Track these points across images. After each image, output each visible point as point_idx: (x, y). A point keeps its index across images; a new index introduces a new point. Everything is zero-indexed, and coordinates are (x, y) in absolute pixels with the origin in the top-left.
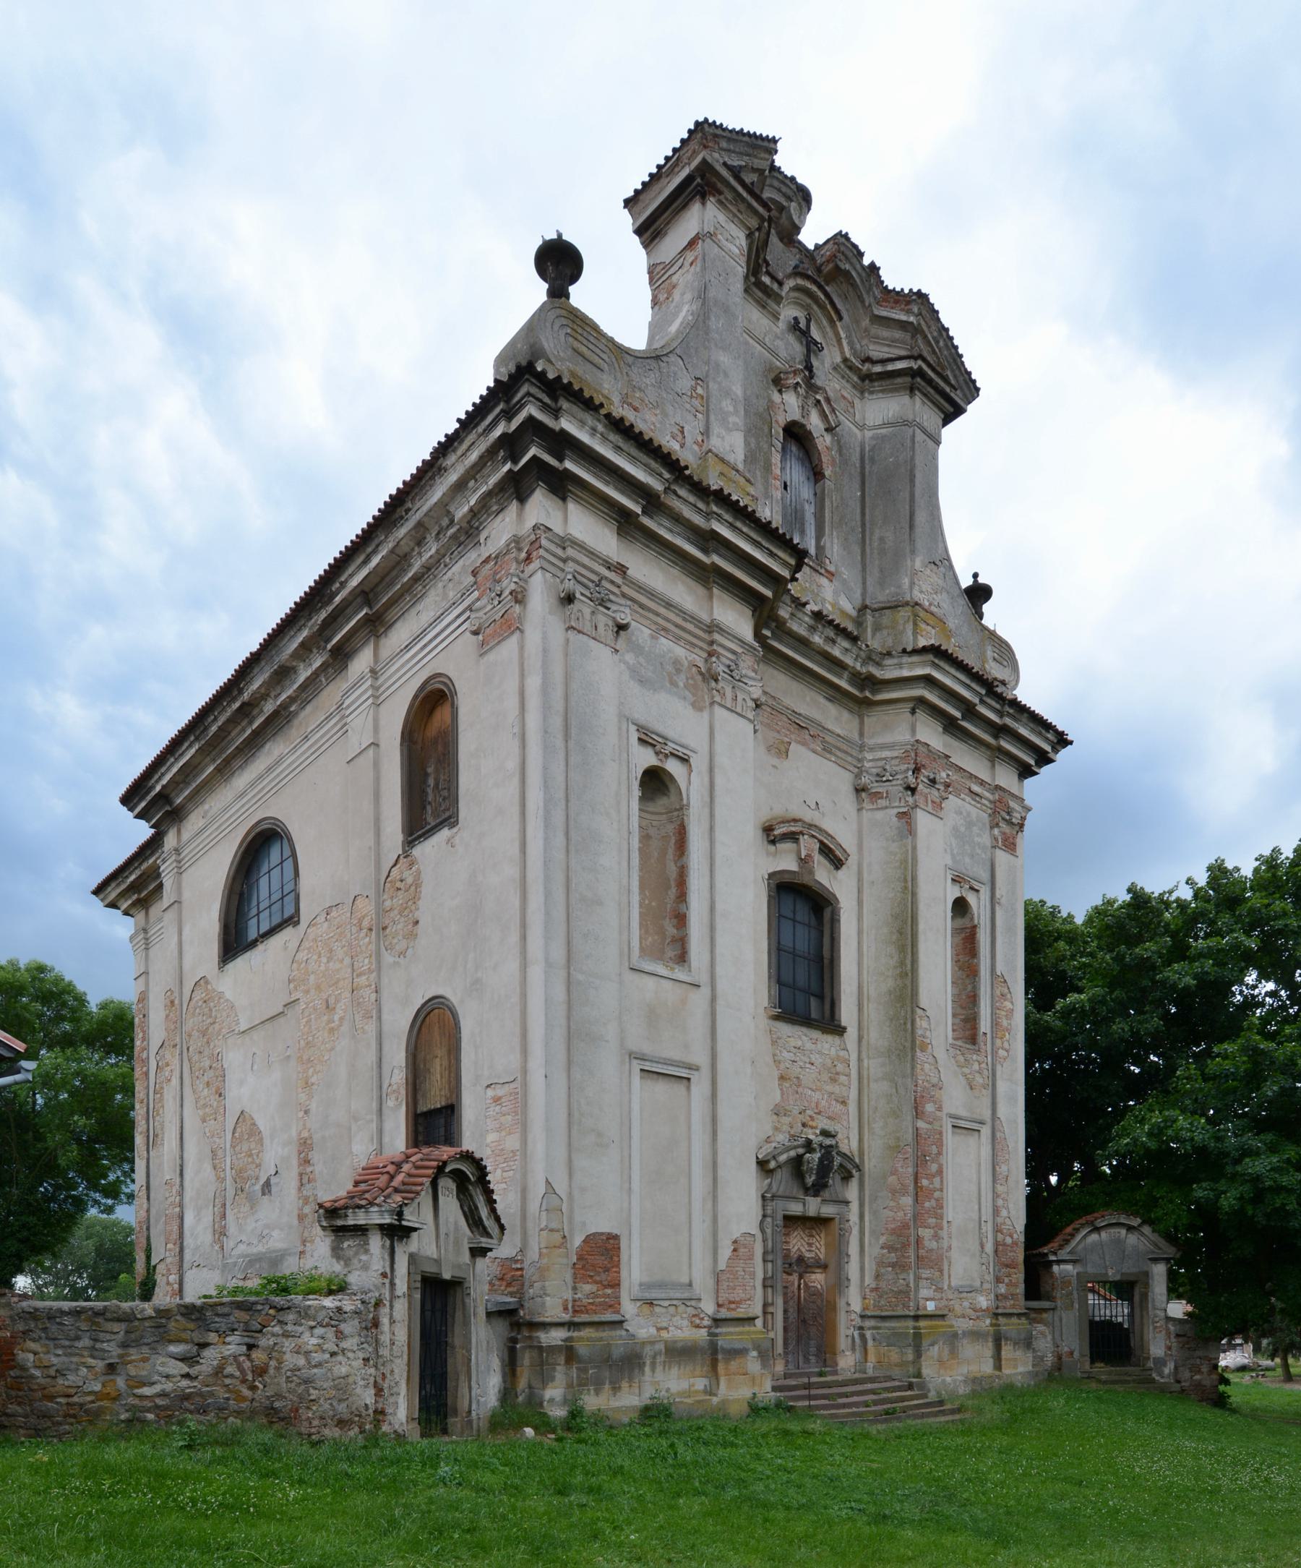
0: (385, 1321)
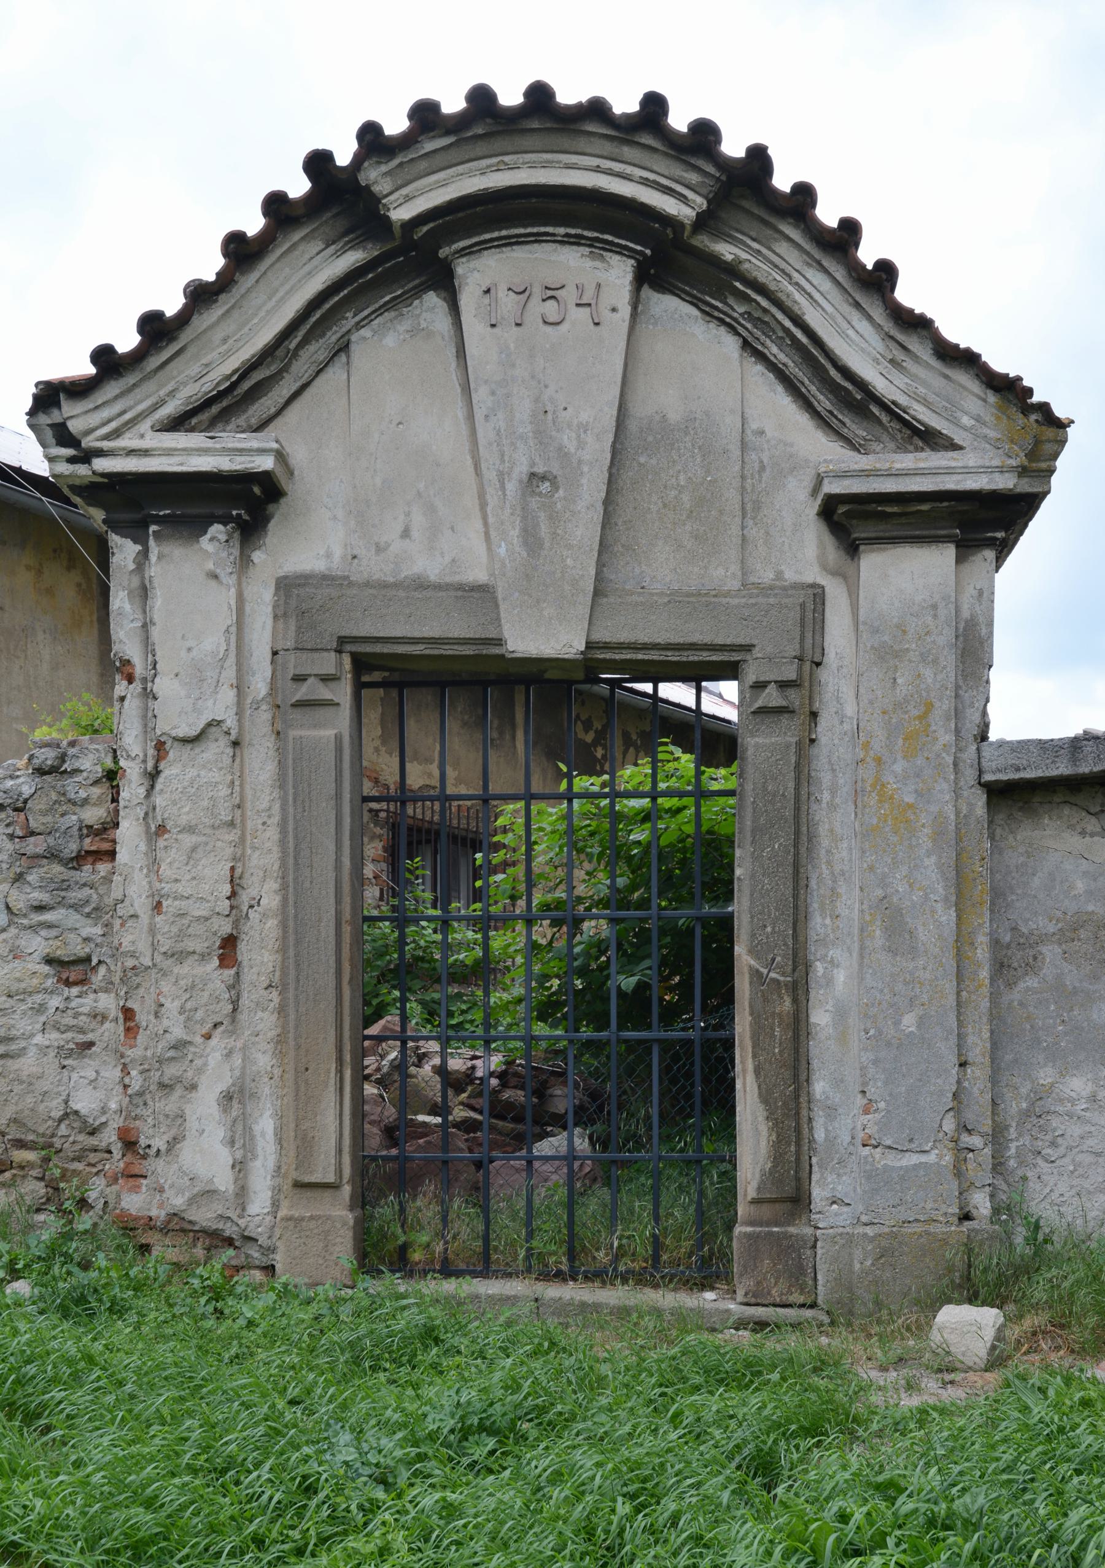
0: (129, 835)
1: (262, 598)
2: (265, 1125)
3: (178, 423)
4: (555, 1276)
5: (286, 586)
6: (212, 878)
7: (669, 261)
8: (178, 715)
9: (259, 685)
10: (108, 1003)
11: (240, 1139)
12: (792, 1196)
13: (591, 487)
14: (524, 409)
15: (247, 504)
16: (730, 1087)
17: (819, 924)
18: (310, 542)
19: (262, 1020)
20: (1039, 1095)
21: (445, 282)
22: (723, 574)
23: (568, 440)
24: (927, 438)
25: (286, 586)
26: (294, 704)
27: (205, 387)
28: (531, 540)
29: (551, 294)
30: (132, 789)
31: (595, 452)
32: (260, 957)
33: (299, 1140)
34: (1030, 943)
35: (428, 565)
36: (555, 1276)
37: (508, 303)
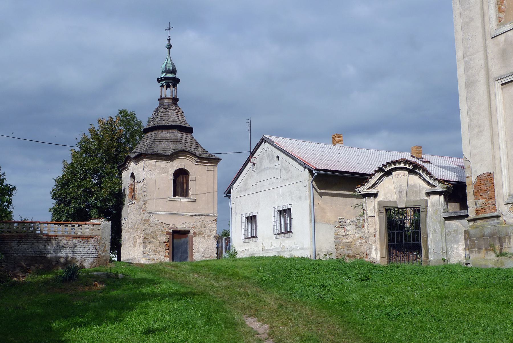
1: (376, 203)
2: (379, 252)
3: (368, 189)
4: (432, 177)
5: (378, 202)
6: (373, 229)
7: (411, 172)
8: (369, 215)
9: (377, 211)
10: (364, 241)
11: (376, 254)
12: (428, 258)
13: (405, 192)
14: (399, 185)
15: (375, 195)
16: (458, 109)
17: (428, 231)
18: (381, 197)
19: (378, 242)
20: (452, 247)
21: (391, 174)
22: (418, 199)
23: (403, 187)
24: (435, 186)
25: (378, 202)
26: (379, 213)
27: (370, 186)
28: (400, 197)
29: (401, 175)
30: (366, 221)
31: (405, 188)
32: (378, 236)
33: (381, 253)
34: (450, 232)
35: (391, 199)
36: (432, 177)
37: (397, 176)
